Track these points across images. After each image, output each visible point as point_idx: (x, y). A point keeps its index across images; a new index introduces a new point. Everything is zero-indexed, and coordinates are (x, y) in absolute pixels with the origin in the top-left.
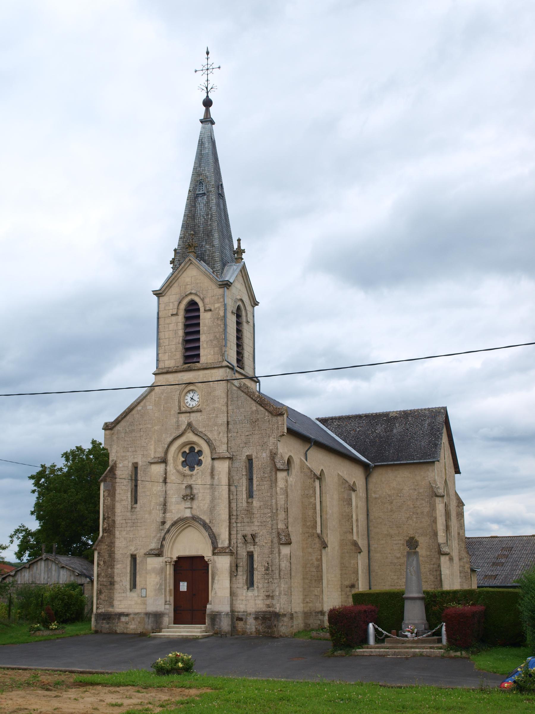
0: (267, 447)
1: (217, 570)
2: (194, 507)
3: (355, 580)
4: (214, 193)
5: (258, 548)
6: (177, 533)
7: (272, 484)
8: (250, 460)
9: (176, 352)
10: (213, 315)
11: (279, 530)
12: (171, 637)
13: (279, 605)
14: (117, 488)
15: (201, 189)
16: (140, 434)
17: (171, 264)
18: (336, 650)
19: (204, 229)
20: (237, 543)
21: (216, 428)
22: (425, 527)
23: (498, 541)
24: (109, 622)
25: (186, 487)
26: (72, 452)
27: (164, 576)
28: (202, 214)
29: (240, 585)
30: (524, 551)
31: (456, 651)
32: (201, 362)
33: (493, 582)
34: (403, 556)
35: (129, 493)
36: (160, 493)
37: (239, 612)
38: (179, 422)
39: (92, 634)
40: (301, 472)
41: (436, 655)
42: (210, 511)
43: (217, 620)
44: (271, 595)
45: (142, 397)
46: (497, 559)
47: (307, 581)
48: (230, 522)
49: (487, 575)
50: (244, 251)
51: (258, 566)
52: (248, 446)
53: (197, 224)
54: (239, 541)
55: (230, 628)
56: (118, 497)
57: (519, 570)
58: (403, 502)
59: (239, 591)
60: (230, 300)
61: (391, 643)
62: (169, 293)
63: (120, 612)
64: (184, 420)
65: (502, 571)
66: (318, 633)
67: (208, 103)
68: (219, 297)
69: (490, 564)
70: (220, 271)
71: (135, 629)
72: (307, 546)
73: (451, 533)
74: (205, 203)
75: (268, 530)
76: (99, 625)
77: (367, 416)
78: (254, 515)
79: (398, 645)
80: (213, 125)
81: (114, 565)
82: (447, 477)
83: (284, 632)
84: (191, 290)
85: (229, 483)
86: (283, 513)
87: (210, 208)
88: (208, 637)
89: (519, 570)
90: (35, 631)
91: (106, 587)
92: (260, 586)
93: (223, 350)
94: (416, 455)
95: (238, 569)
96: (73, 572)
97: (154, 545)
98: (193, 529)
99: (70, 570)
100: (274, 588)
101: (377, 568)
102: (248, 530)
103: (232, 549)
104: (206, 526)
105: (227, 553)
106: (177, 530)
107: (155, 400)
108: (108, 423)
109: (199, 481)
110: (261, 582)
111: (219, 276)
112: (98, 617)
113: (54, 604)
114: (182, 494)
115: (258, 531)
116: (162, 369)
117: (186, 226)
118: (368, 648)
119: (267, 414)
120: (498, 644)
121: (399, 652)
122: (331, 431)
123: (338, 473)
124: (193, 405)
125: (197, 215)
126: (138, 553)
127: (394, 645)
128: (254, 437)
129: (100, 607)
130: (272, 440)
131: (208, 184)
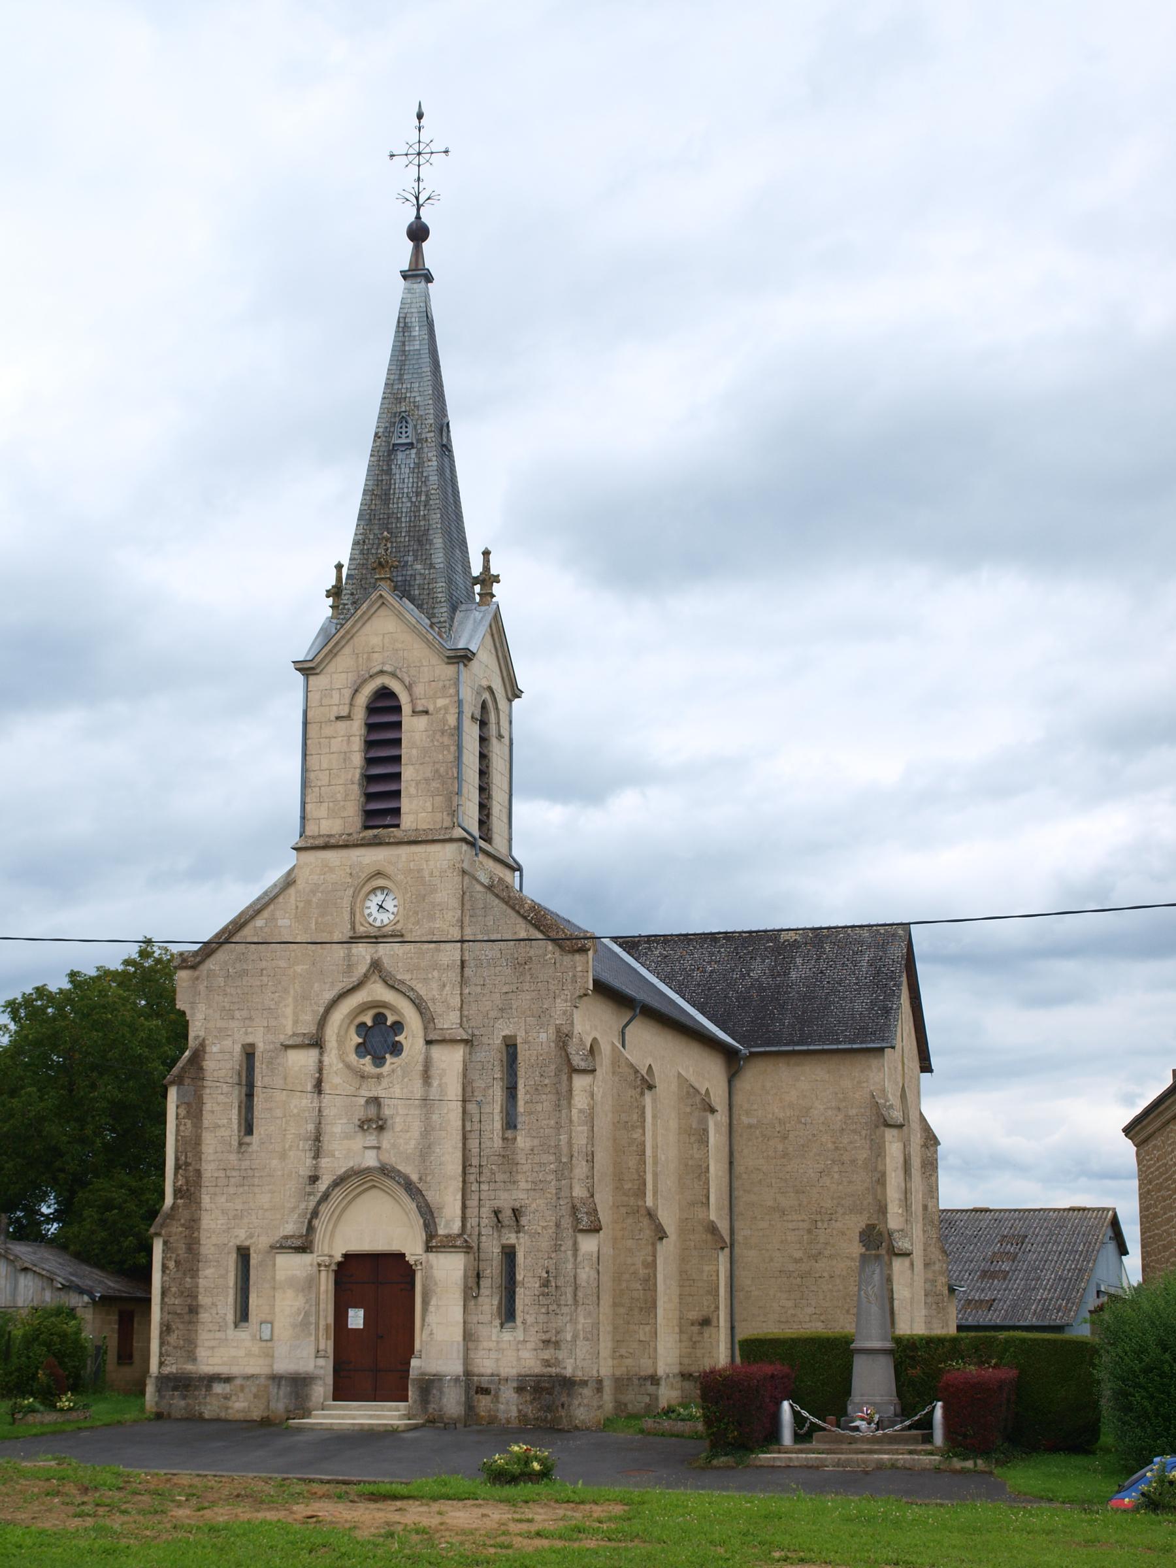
0: (549, 1021)
1: (436, 1284)
2: (384, 1147)
3: (712, 1308)
4: (433, 444)
5: (527, 1237)
6: (345, 1202)
7: (559, 1100)
8: (511, 1048)
9: (345, 801)
10: (432, 724)
11: (576, 1201)
12: (335, 1427)
13: (572, 1361)
14: (206, 1099)
15: (404, 432)
16: (261, 981)
17: (328, 596)
18: (715, 1456)
19: (410, 526)
20: (479, 1225)
21: (436, 973)
22: (860, 1193)
23: (990, 1221)
24: (186, 1396)
25: (367, 1102)
26: (27, 1001)
27: (313, 1296)
28: (406, 490)
29: (486, 1318)
30: (1054, 1244)
31: (965, 1459)
32: (403, 826)
33: (987, 1316)
34: (809, 1257)
35: (235, 1111)
36: (307, 1114)
37: (483, 1376)
38: (353, 958)
39: (149, 1420)
40: (614, 1073)
41: (923, 1466)
42: (421, 1156)
43: (435, 1391)
44: (554, 1339)
45: (267, 898)
46: (992, 1262)
47: (622, 1310)
48: (464, 1182)
49: (972, 1300)
50: (496, 579)
51: (524, 1276)
52: (508, 1016)
53: (393, 513)
54: (484, 1222)
55: (463, 1409)
56: (207, 1120)
57: (1044, 1290)
58: (810, 1137)
59: (483, 1331)
60: (469, 690)
61: (825, 1442)
62: (331, 668)
63: (211, 1372)
64: (364, 953)
65: (1005, 1290)
66: (658, 1423)
67: (418, 233)
68: (447, 683)
69: (976, 1274)
70: (447, 625)
71: (247, 1410)
72: (623, 1235)
73: (911, 1207)
74: (412, 466)
75: (549, 1200)
76: (165, 1401)
77: (728, 936)
78: (519, 1167)
79: (841, 1447)
80: (429, 284)
81: (198, 1270)
82: (906, 1080)
83: (583, 1420)
84: (383, 663)
85: (464, 1095)
86: (584, 1163)
87: (423, 479)
88: (415, 1428)
89: (1044, 1290)
90: (25, 1414)
91: (180, 1318)
92: (530, 1320)
93: (455, 804)
94: (842, 1032)
95: (481, 1283)
96: (50, 1282)
97: (291, 1227)
98: (381, 1194)
99: (43, 1275)
100: (560, 1324)
101: (749, 1282)
102: (504, 1199)
103: (468, 1239)
104: (411, 1189)
105: (460, 1247)
106: (346, 1195)
107: (297, 907)
108: (187, 954)
109: (397, 1091)
110: (531, 1312)
111: (445, 636)
112: (162, 1383)
113: (31, 1354)
114: (358, 1117)
115: (527, 1201)
116: (313, 837)
117: (367, 517)
118: (779, 1452)
119: (550, 948)
120: (1042, 1448)
121: (847, 1460)
122: (648, 969)
123: (679, 1073)
124: (382, 921)
125: (394, 493)
126: (254, 1243)
127: (834, 1447)
128: (520, 997)
129: (166, 1362)
130: (561, 1005)
131: (419, 422)
